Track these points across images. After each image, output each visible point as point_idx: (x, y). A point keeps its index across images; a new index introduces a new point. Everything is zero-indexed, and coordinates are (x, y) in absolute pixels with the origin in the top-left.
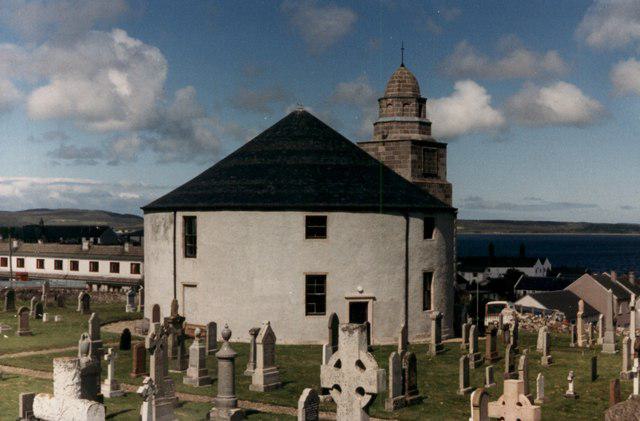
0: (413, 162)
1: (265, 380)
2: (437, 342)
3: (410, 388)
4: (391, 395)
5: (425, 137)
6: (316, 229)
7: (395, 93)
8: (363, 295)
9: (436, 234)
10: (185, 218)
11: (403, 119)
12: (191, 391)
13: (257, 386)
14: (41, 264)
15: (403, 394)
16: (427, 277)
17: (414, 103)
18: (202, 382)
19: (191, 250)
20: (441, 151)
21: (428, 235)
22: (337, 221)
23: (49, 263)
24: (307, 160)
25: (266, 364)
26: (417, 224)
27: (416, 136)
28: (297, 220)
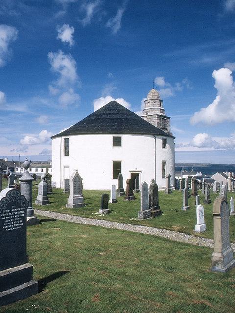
0: (158, 123)
1: (74, 202)
2: (168, 187)
3: (154, 205)
4: (142, 210)
5: (162, 114)
6: (117, 142)
7: (151, 98)
8: (136, 170)
9: (167, 145)
10: (65, 139)
11: (153, 107)
12: (39, 208)
13: (69, 205)
14: (37, 170)
15: (150, 209)
16: (164, 163)
17: (158, 102)
18: (44, 203)
19: (67, 153)
20: (168, 120)
21: (164, 146)
22: (126, 138)
23: (39, 169)
24: (115, 117)
25: (75, 193)
26: (159, 141)
27: (159, 114)
28: (109, 138)
